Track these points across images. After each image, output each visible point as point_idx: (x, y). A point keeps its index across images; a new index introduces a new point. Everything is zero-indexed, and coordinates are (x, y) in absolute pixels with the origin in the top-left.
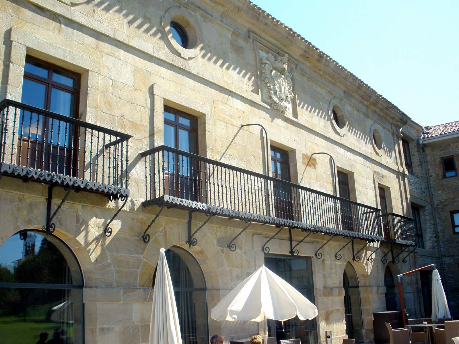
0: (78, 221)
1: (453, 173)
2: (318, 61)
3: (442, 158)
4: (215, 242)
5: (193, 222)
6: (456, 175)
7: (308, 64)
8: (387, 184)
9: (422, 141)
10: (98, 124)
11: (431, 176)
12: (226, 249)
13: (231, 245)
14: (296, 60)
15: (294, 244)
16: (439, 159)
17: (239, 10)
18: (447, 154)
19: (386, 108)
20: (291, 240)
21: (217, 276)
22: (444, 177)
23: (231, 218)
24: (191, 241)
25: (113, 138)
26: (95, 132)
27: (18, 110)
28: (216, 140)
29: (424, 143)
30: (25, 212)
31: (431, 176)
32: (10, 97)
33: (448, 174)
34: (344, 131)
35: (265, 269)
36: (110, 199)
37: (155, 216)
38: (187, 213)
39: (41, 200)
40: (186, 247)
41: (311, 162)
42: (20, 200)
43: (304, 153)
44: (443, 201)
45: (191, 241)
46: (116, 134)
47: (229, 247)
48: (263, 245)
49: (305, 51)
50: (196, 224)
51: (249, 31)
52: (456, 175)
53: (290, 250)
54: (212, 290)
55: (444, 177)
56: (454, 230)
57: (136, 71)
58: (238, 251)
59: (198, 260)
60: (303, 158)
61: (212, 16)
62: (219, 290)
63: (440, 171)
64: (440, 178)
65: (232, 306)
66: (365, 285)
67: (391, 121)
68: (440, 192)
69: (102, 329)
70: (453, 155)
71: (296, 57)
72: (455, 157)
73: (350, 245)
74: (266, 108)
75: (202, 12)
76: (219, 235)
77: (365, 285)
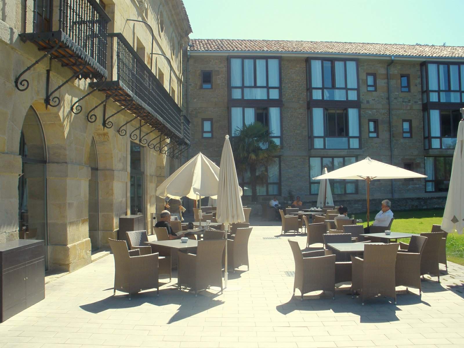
1: (209, 86)
3: (202, 70)
6: (212, 88)
9: (190, 53)
11: (190, 85)
16: (200, 71)
21: (112, 157)
22: (201, 88)
27: (441, 67)
29: (191, 54)
31: (190, 85)
33: (205, 86)
34: (162, 34)
35: (201, 155)
36: (78, 77)
44: (197, 108)
48: (130, 134)
52: (212, 88)
54: (105, 170)
55: (201, 88)
56: (202, 135)
59: (96, 141)
62: (114, 171)
63: (199, 82)
64: (198, 88)
65: (194, 184)
66: (161, 175)
67: (180, 30)
68: (195, 100)
70: (212, 71)
72: (213, 72)
74: (137, 5)
77: (161, 175)
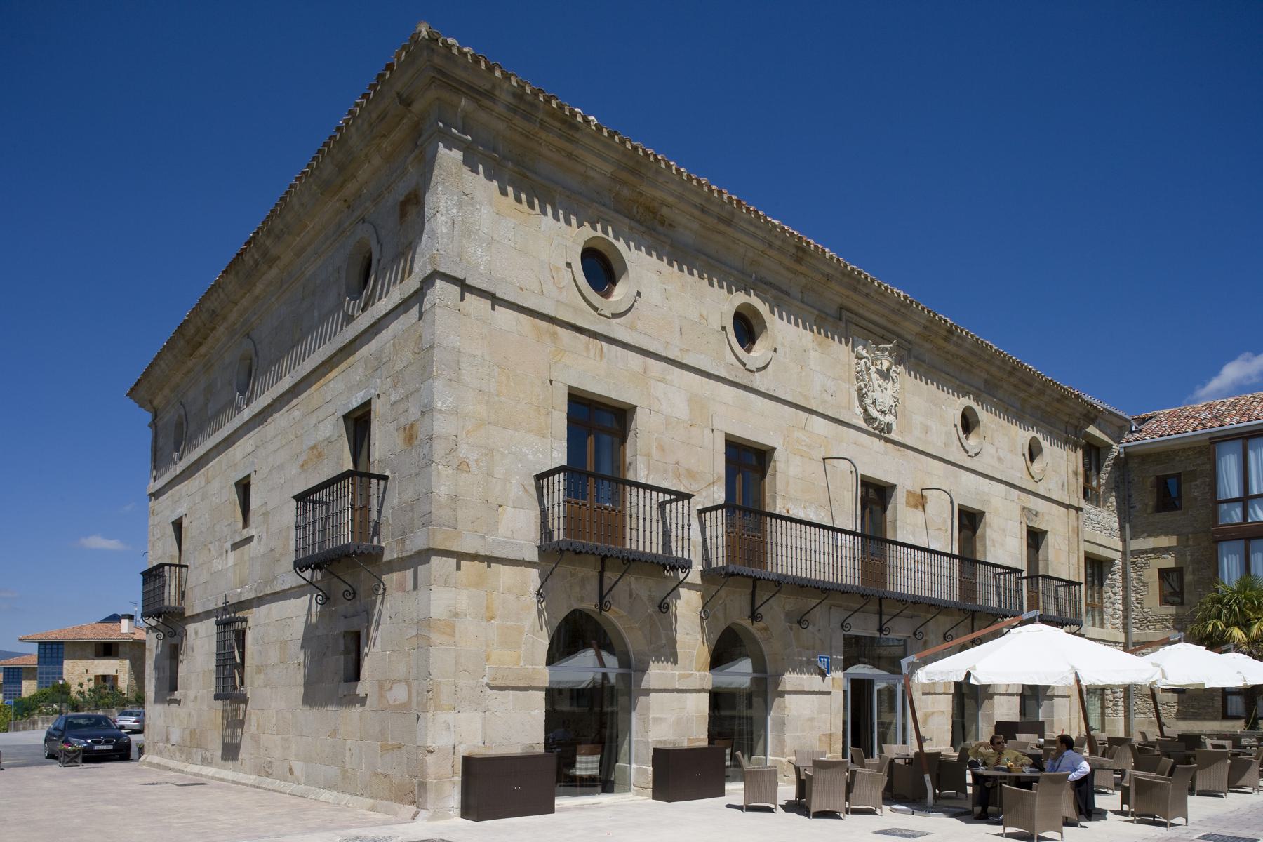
0: (631, 596)
2: (946, 339)
4: (783, 616)
5: (758, 592)
7: (928, 346)
8: (1042, 527)
10: (650, 482)
12: (795, 626)
13: (802, 621)
14: (909, 342)
15: (884, 619)
17: (829, 277)
18: (1161, 470)
19: (1058, 401)
20: (880, 613)
23: (802, 587)
24: (754, 617)
25: (668, 497)
26: (648, 492)
28: (788, 483)
30: (578, 589)
32: (555, 454)
37: (741, 803)
38: (750, 582)
39: (591, 573)
40: (747, 623)
41: (920, 501)
42: (572, 575)
43: (910, 489)
45: (754, 617)
46: (670, 492)
47: (799, 622)
49: (925, 328)
50: (761, 596)
51: (842, 308)
53: (877, 627)
57: (695, 401)
58: (810, 627)
60: (908, 498)
61: (416, 587)
69: (656, 720)
71: (909, 337)
73: (968, 621)
75: (774, 292)
76: (787, 607)
